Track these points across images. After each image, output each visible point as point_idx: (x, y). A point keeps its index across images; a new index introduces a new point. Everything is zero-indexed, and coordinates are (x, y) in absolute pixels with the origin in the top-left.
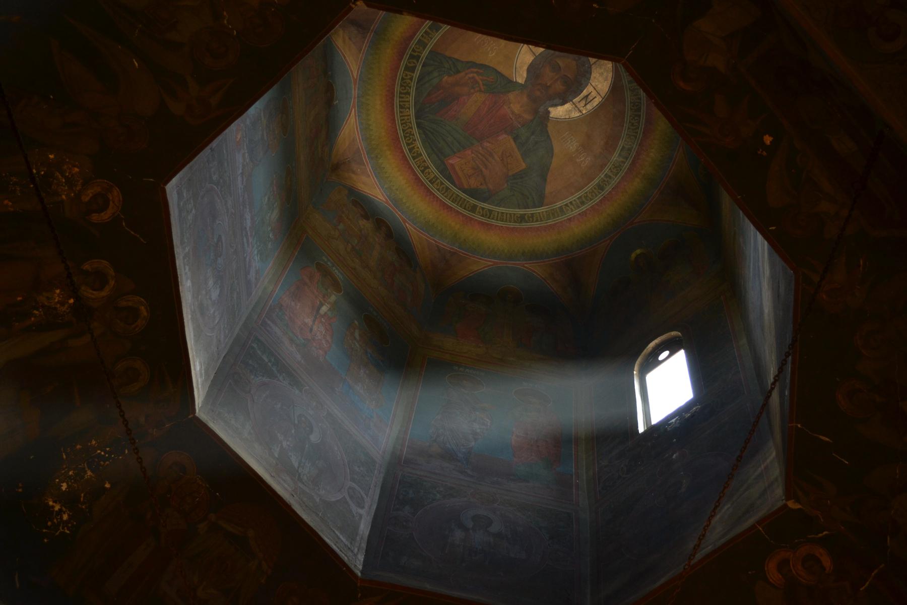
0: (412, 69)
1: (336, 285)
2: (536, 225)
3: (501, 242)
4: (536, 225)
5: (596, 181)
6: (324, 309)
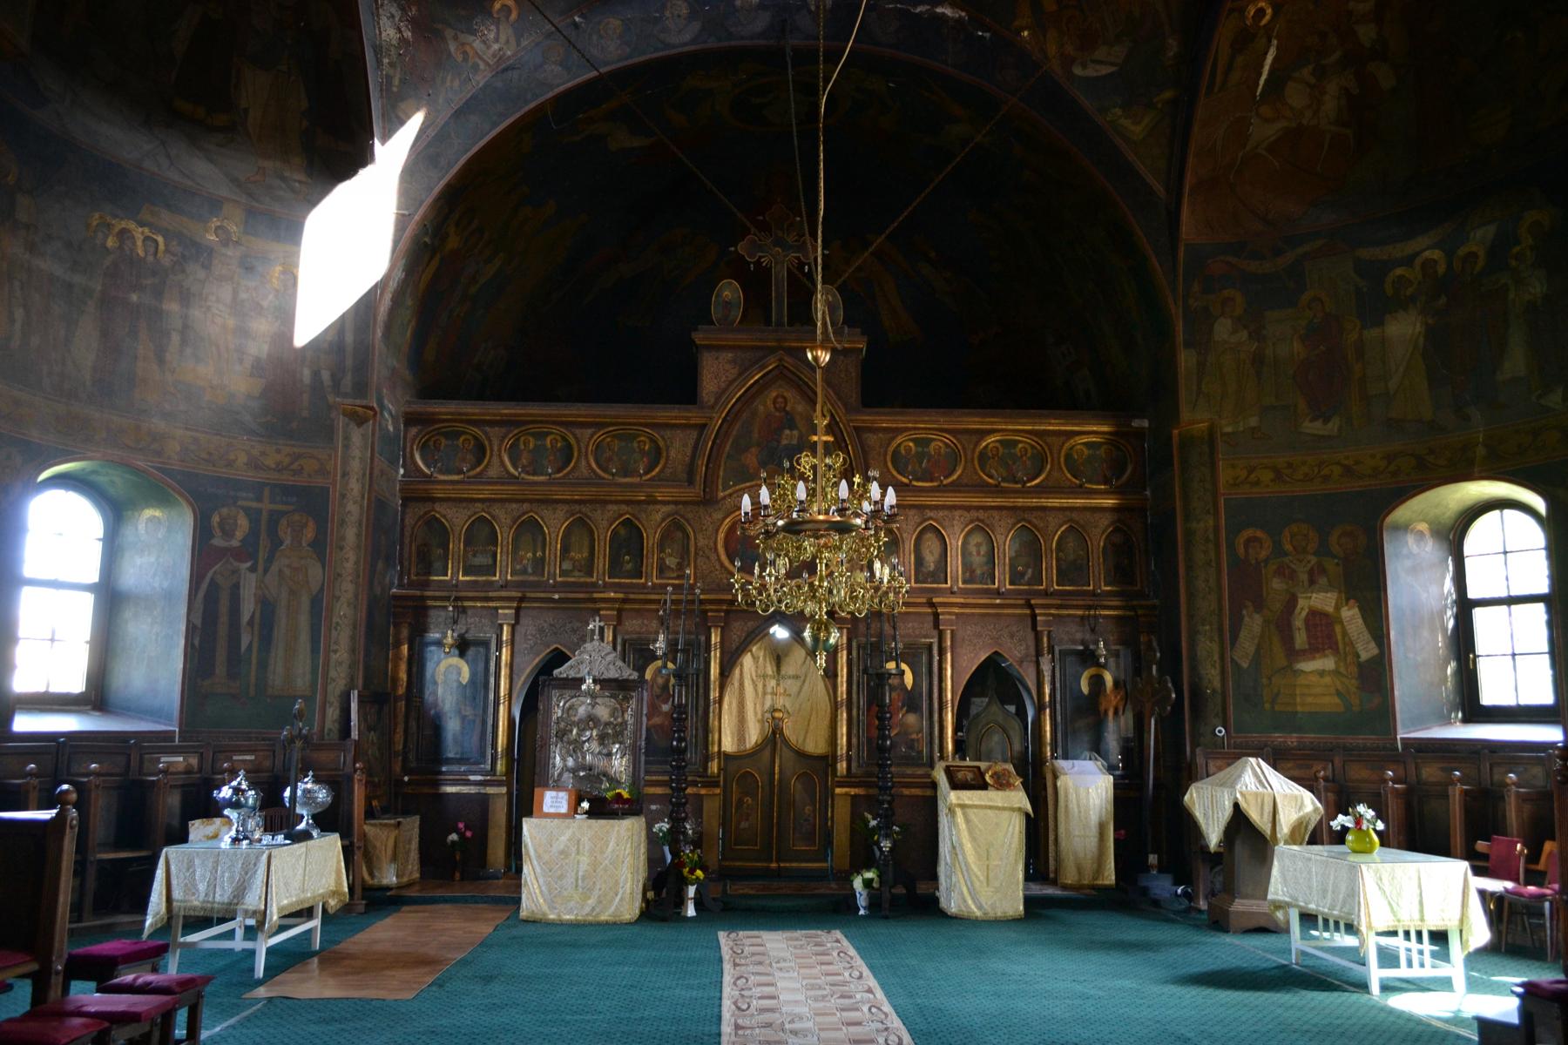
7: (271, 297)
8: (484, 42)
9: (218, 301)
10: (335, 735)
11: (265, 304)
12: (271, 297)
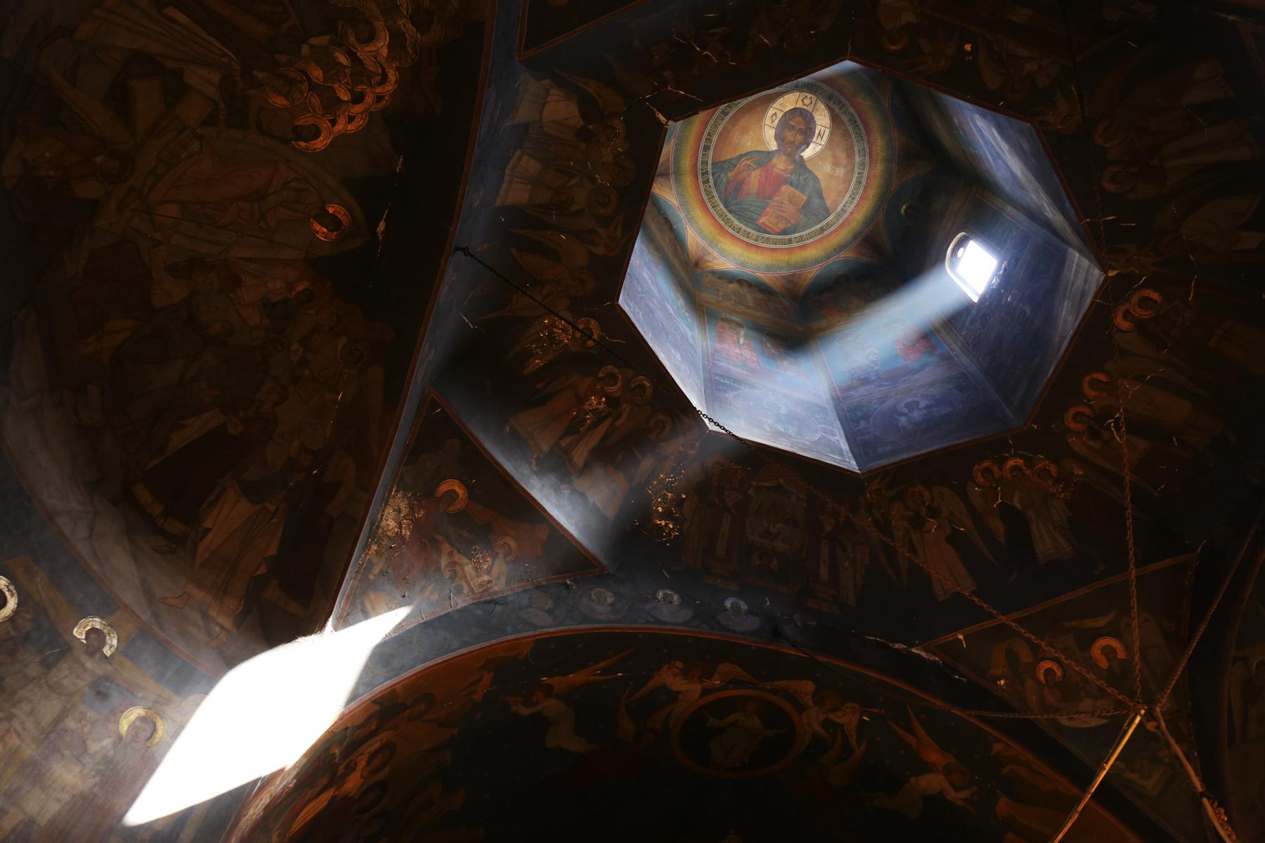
0: (708, 181)
1: (739, 325)
2: (832, 228)
3: (816, 251)
4: (832, 228)
5: (854, 180)
6: (742, 341)
7: (107, 742)
8: (476, 569)
9: (31, 713)
10: (101, 689)
11: (94, 747)
12: (107, 742)
